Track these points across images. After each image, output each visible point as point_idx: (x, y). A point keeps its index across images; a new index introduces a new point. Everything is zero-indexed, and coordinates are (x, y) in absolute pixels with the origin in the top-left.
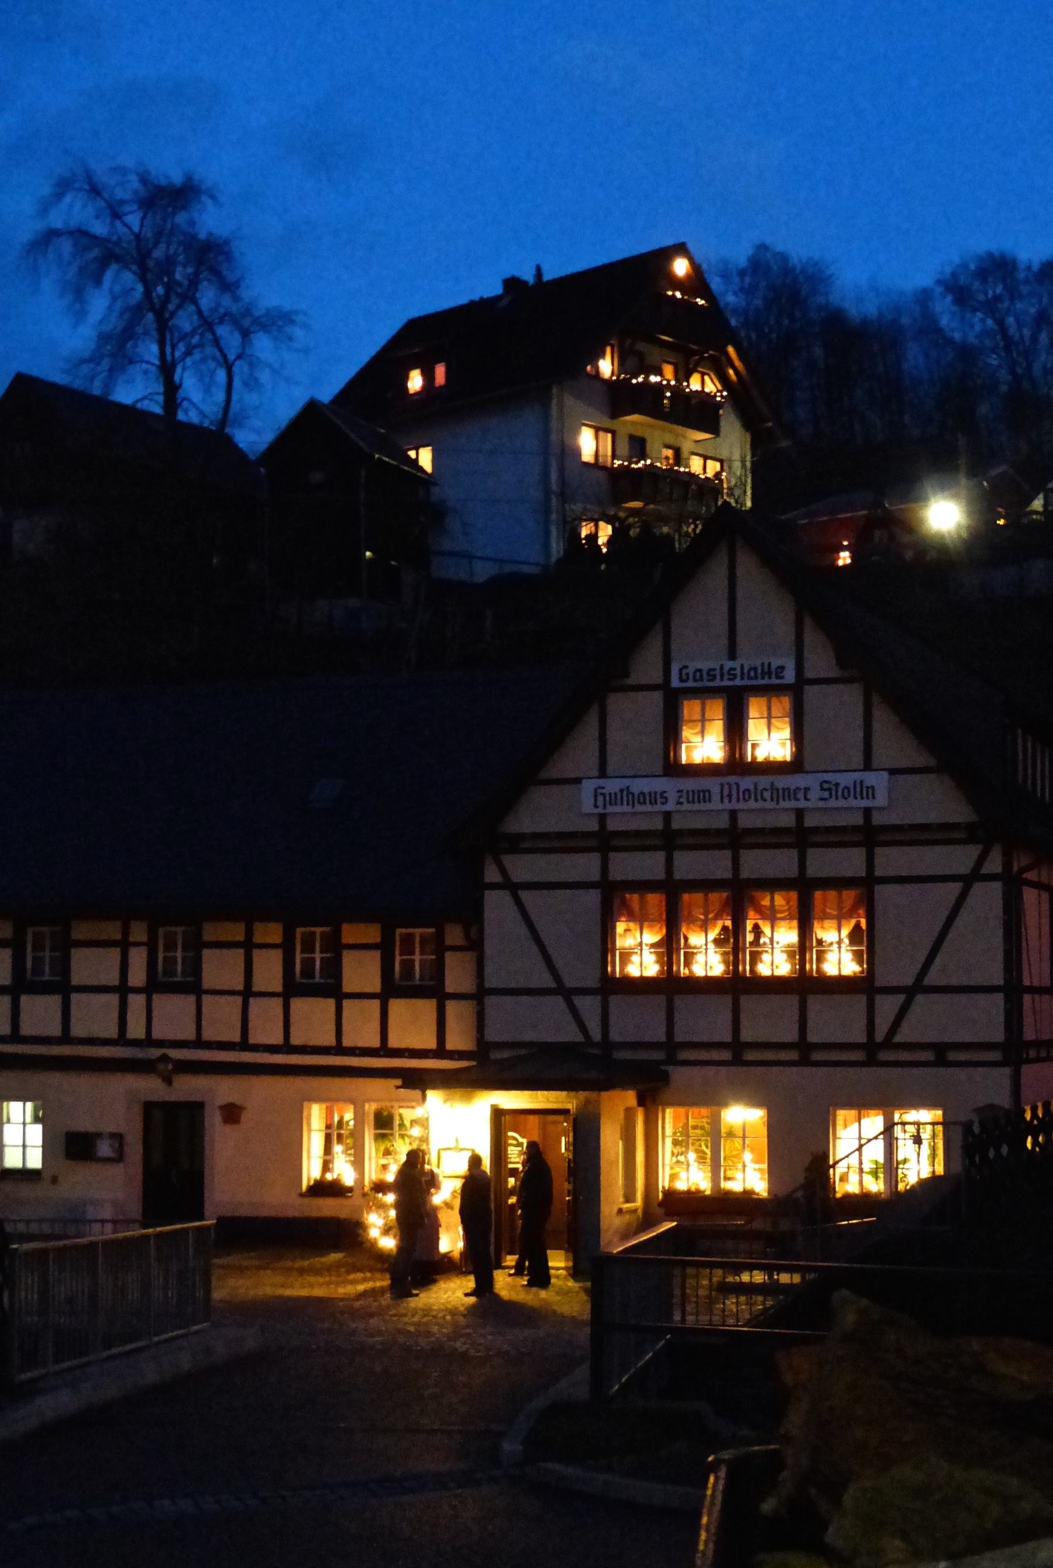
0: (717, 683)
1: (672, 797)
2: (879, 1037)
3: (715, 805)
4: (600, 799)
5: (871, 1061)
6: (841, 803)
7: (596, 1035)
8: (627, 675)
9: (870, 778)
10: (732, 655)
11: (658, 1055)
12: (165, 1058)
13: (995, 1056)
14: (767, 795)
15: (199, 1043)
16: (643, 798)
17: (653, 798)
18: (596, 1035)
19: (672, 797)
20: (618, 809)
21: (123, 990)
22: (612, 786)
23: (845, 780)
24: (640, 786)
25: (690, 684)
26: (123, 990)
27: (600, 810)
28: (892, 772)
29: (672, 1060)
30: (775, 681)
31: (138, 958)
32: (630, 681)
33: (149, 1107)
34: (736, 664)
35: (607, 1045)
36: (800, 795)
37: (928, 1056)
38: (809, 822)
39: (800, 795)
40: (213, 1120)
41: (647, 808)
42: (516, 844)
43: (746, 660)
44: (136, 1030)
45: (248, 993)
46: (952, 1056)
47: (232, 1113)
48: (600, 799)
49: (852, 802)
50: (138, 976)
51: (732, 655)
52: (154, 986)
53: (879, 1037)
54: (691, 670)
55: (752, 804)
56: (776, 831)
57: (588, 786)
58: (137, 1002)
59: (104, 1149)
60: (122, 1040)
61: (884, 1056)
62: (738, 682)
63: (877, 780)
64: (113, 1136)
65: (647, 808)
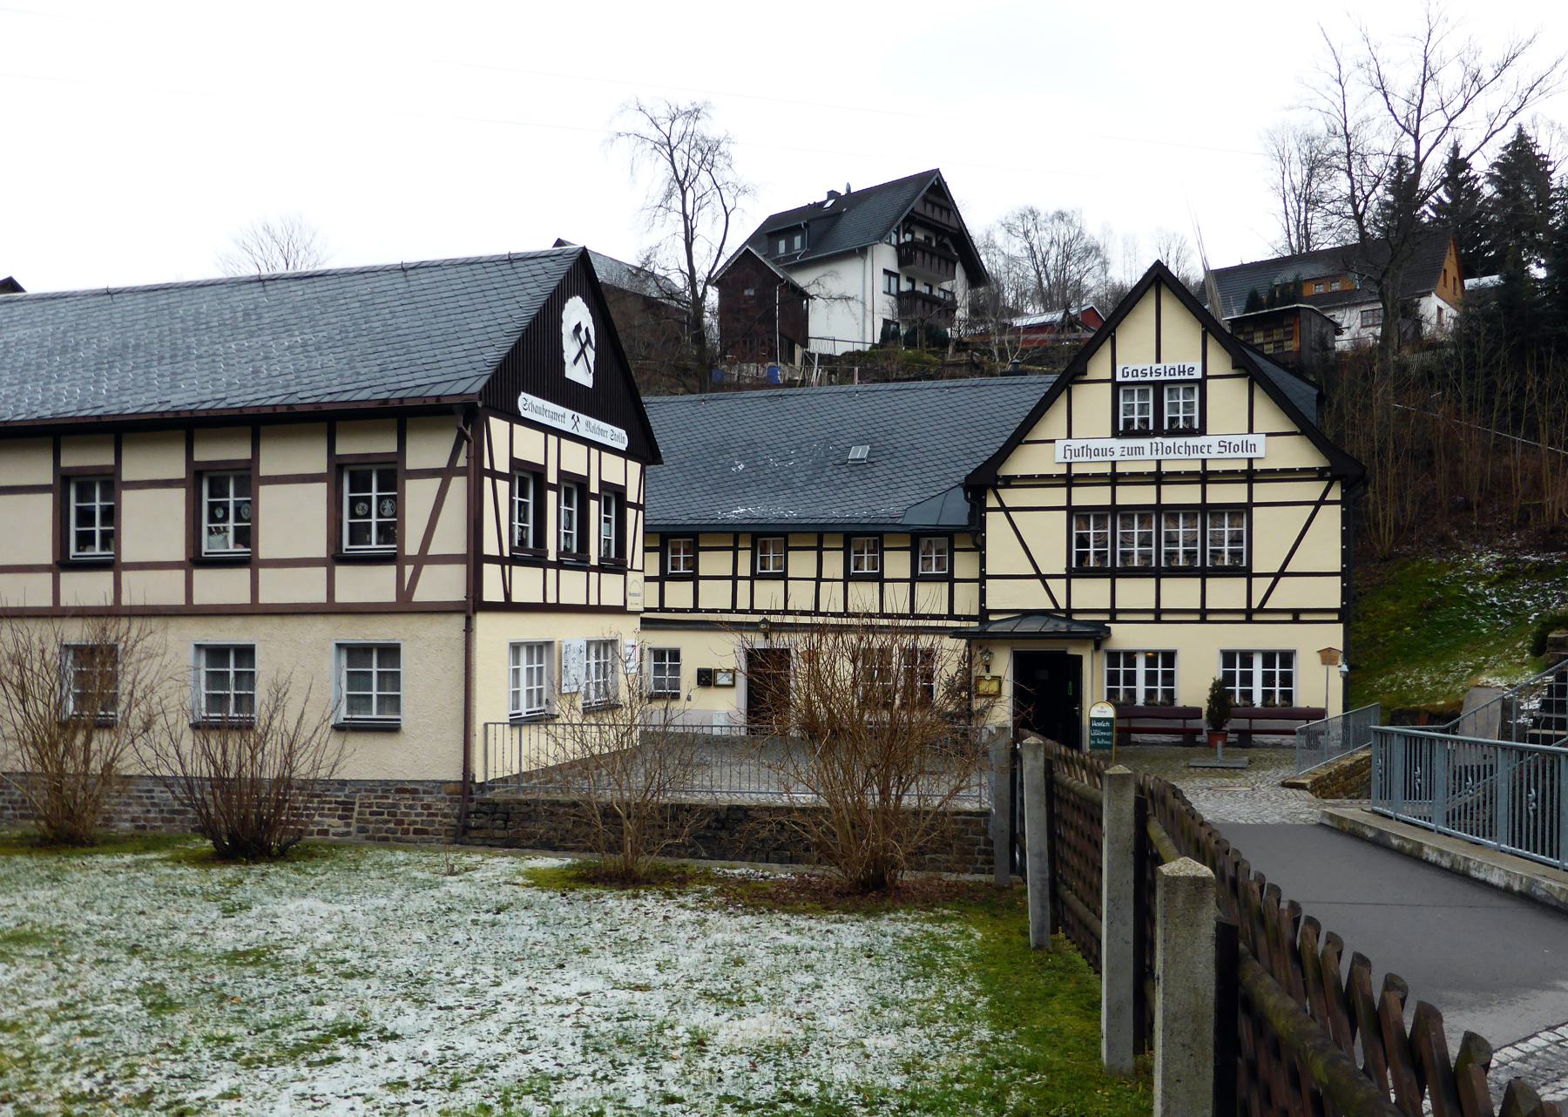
0: (1148, 378)
1: (1118, 452)
2: (1255, 605)
3: (1147, 455)
4: (1068, 453)
5: (1249, 621)
6: (1233, 455)
7: (1063, 606)
8: (1085, 373)
9: (1251, 439)
10: (1158, 360)
11: (1106, 617)
12: (764, 621)
13: (1335, 617)
14: (1182, 450)
15: (786, 612)
16: (1097, 452)
17: (1104, 452)
18: (1063, 606)
19: (1118, 452)
20: (1080, 459)
21: (735, 578)
22: (1076, 444)
23: (1236, 440)
24: (1093, 444)
25: (1130, 379)
26: (735, 578)
27: (1068, 460)
28: (1268, 435)
29: (1113, 620)
30: (1187, 377)
31: (745, 559)
32: (1086, 378)
33: (751, 655)
34: (1160, 366)
35: (1070, 611)
36: (1205, 450)
37: (1289, 617)
38: (1211, 467)
39: (1205, 450)
41: (1100, 458)
42: (1009, 482)
43: (1167, 362)
44: (743, 603)
45: (819, 579)
46: (1303, 617)
48: (1068, 453)
49: (1240, 454)
50: (744, 569)
51: (1158, 360)
52: (754, 577)
53: (1255, 605)
54: (1130, 371)
55: (1172, 456)
56: (1188, 473)
57: (1060, 445)
58: (744, 586)
59: (723, 679)
60: (734, 609)
61: (1256, 617)
62: (1162, 378)
63: (1258, 440)
64: (728, 671)
65: (1100, 458)
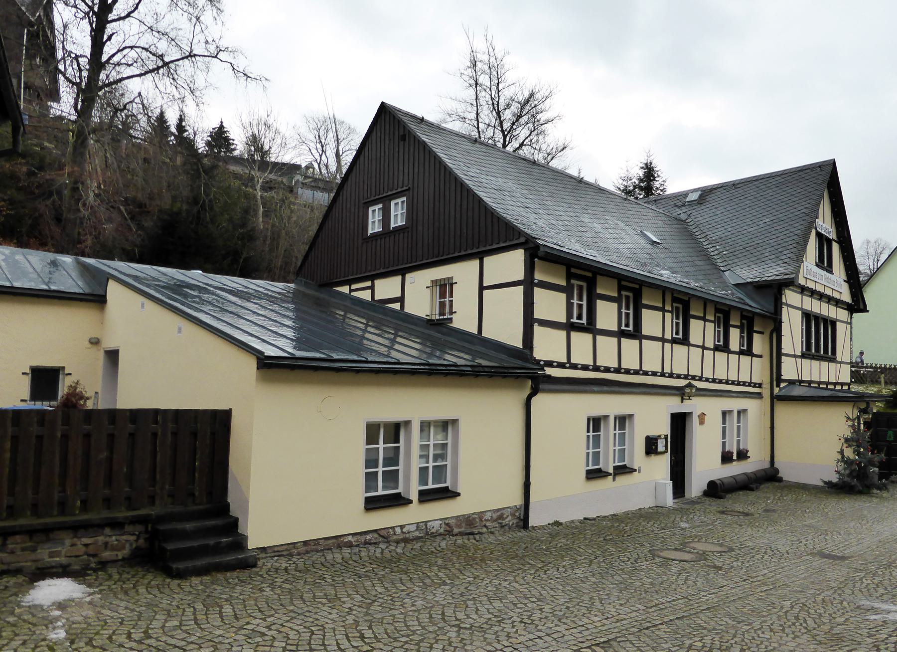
26: (704, 348)
40: (695, 419)
47: (702, 416)
